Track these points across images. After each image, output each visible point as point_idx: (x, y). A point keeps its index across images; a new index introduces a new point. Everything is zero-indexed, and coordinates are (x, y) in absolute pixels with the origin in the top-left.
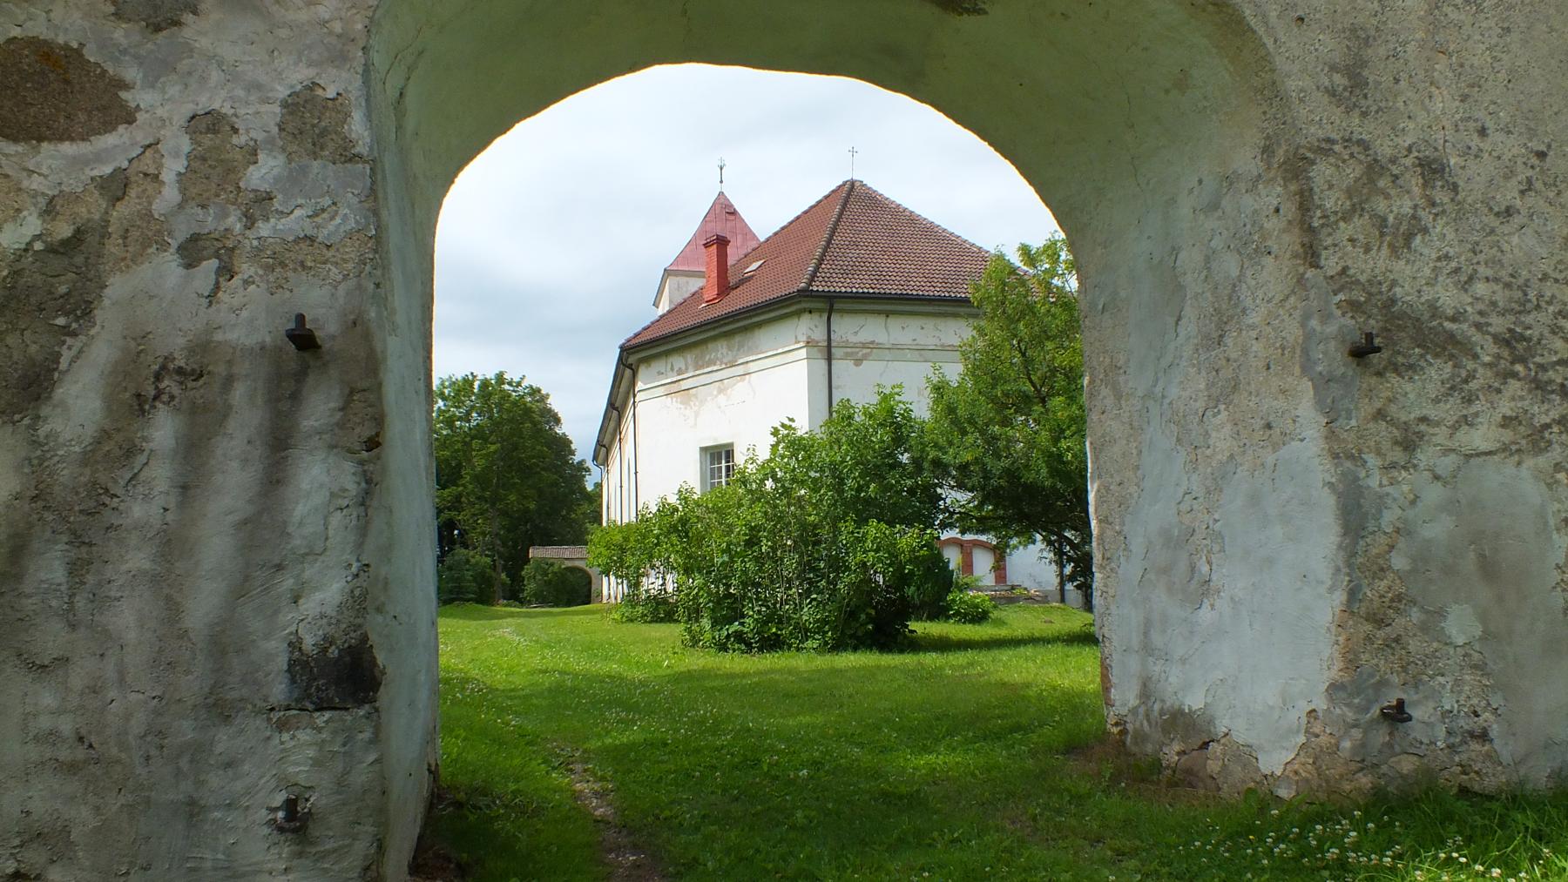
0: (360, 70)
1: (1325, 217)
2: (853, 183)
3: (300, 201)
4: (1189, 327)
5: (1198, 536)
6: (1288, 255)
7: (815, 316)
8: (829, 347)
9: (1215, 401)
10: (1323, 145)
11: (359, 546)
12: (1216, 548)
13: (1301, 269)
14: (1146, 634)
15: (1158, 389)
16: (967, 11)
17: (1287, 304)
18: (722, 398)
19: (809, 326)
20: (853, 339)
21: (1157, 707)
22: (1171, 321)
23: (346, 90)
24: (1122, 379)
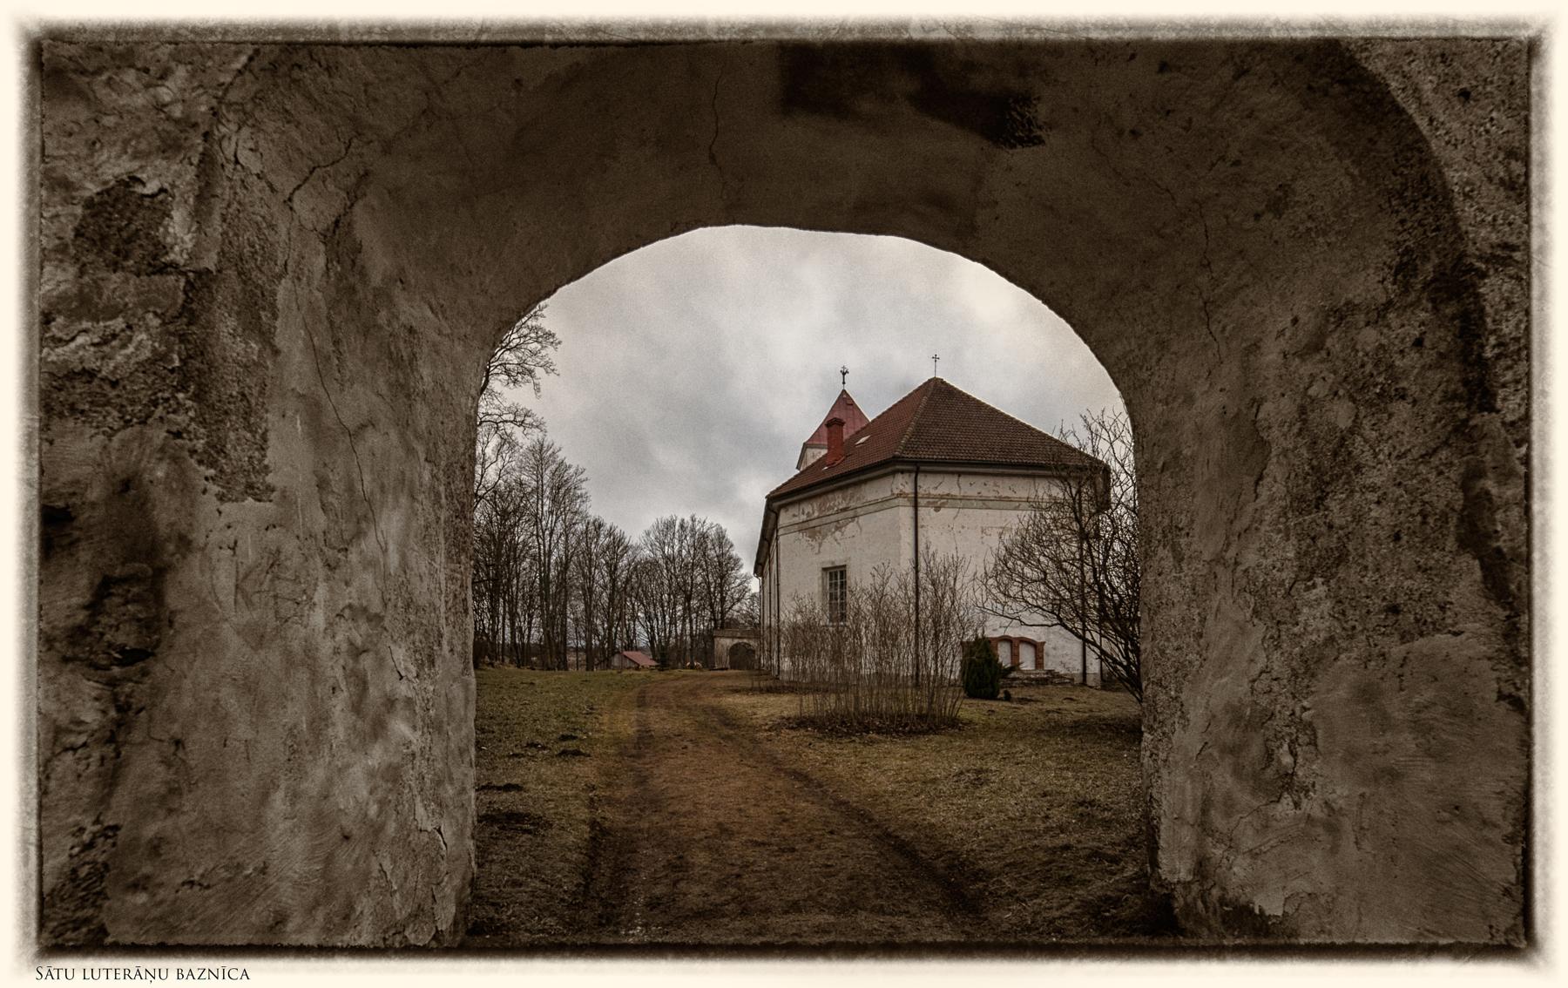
0: (195, 161)
1: (1499, 345)
2: (935, 380)
3: (86, 324)
4: (1276, 484)
5: (1277, 723)
6: (1437, 397)
7: (906, 476)
8: (916, 497)
9: (1308, 573)
10: (1499, 252)
11: (103, 801)
12: (1303, 739)
13: (1463, 415)
14: (1204, 812)
15: (1231, 554)
16: (1022, 142)
17: (1435, 461)
18: (838, 534)
19: (902, 484)
20: (933, 492)
21: (1216, 892)
22: (1252, 480)
23: (173, 186)
24: (1183, 541)
